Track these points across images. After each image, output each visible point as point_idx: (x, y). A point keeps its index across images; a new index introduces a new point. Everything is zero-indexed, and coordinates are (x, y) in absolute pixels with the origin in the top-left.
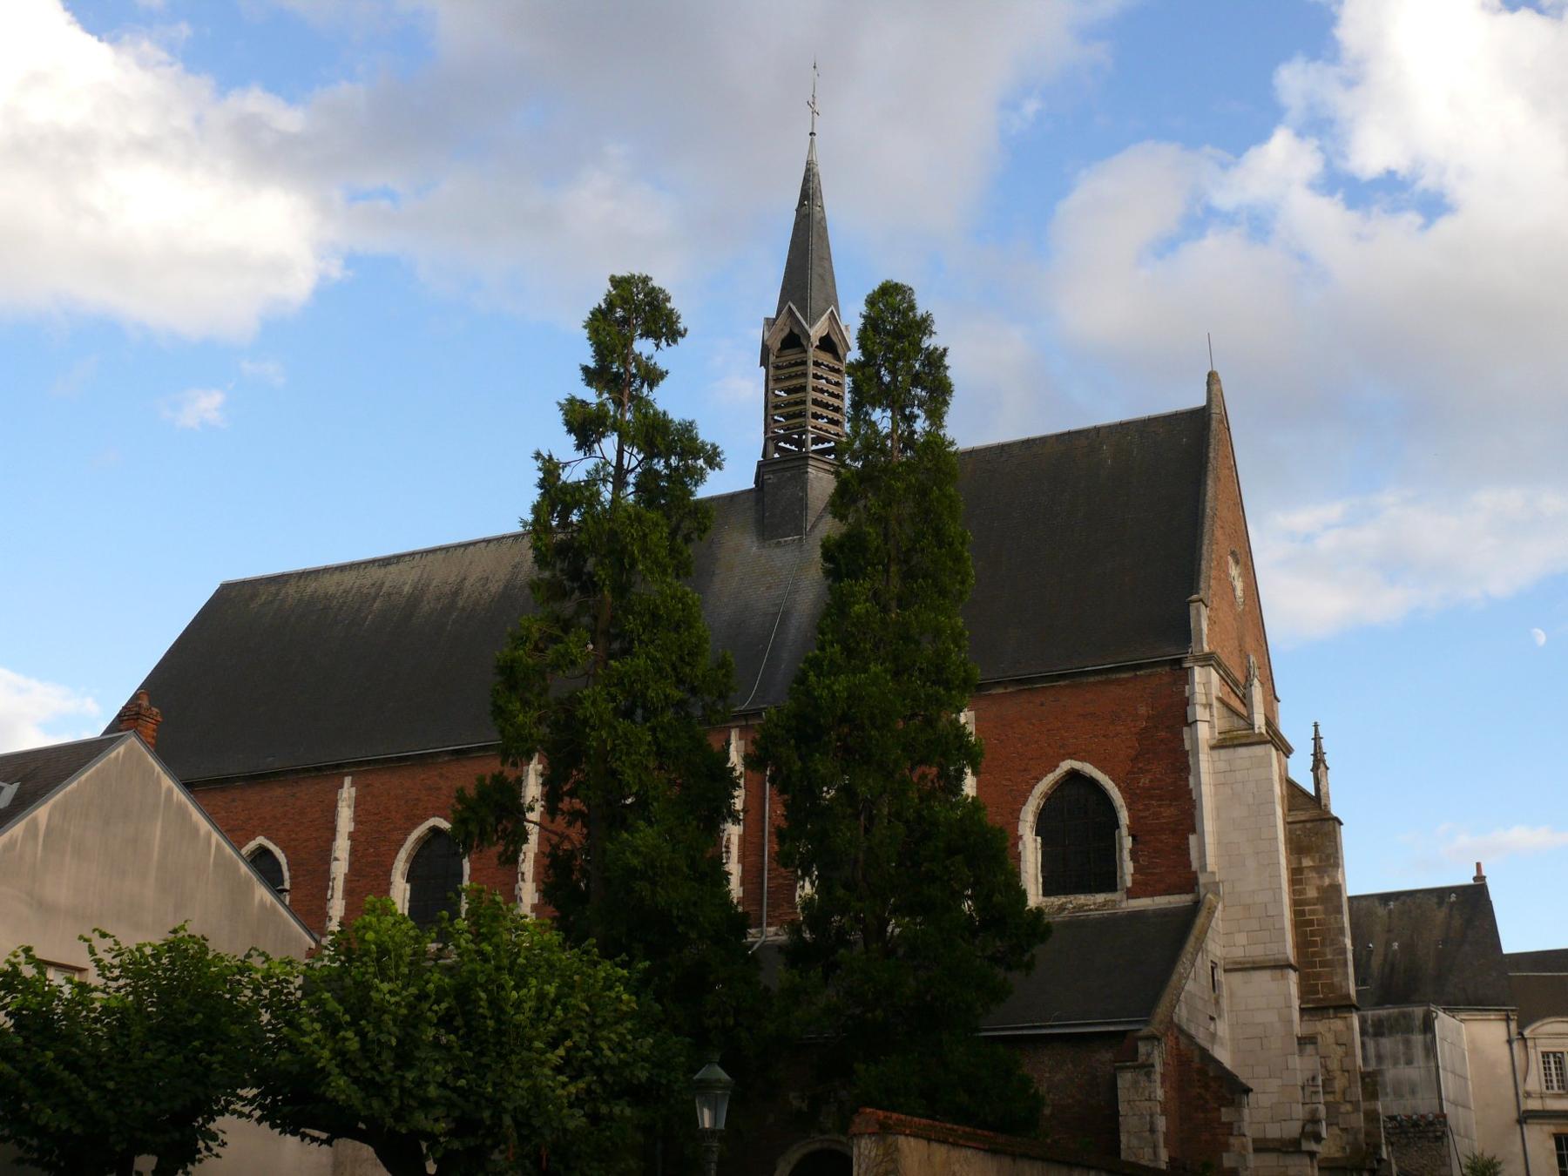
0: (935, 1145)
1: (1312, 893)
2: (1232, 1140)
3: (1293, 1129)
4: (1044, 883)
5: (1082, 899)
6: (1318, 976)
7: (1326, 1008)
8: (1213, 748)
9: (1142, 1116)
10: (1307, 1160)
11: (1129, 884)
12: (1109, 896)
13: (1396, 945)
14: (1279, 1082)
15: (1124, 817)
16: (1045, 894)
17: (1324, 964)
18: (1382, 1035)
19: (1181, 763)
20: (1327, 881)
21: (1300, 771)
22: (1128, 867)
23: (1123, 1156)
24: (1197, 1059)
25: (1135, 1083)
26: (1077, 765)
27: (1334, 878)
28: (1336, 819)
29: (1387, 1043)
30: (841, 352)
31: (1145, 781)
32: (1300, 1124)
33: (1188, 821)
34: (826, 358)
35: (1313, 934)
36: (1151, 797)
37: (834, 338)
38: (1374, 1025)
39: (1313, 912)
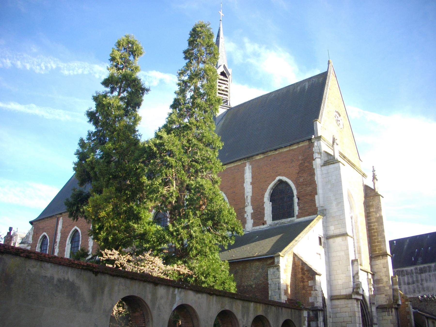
0: (258, 304)
2: (312, 292)
3: (349, 291)
5: (284, 220)
6: (376, 246)
7: (379, 256)
8: (322, 166)
9: (275, 284)
10: (355, 301)
15: (295, 193)
17: (378, 242)
18: (422, 273)
19: (312, 173)
20: (378, 215)
23: (269, 298)
29: (423, 275)
31: (301, 180)
33: (314, 192)
34: (222, 77)
36: (303, 185)
38: (420, 270)
39: (374, 226)
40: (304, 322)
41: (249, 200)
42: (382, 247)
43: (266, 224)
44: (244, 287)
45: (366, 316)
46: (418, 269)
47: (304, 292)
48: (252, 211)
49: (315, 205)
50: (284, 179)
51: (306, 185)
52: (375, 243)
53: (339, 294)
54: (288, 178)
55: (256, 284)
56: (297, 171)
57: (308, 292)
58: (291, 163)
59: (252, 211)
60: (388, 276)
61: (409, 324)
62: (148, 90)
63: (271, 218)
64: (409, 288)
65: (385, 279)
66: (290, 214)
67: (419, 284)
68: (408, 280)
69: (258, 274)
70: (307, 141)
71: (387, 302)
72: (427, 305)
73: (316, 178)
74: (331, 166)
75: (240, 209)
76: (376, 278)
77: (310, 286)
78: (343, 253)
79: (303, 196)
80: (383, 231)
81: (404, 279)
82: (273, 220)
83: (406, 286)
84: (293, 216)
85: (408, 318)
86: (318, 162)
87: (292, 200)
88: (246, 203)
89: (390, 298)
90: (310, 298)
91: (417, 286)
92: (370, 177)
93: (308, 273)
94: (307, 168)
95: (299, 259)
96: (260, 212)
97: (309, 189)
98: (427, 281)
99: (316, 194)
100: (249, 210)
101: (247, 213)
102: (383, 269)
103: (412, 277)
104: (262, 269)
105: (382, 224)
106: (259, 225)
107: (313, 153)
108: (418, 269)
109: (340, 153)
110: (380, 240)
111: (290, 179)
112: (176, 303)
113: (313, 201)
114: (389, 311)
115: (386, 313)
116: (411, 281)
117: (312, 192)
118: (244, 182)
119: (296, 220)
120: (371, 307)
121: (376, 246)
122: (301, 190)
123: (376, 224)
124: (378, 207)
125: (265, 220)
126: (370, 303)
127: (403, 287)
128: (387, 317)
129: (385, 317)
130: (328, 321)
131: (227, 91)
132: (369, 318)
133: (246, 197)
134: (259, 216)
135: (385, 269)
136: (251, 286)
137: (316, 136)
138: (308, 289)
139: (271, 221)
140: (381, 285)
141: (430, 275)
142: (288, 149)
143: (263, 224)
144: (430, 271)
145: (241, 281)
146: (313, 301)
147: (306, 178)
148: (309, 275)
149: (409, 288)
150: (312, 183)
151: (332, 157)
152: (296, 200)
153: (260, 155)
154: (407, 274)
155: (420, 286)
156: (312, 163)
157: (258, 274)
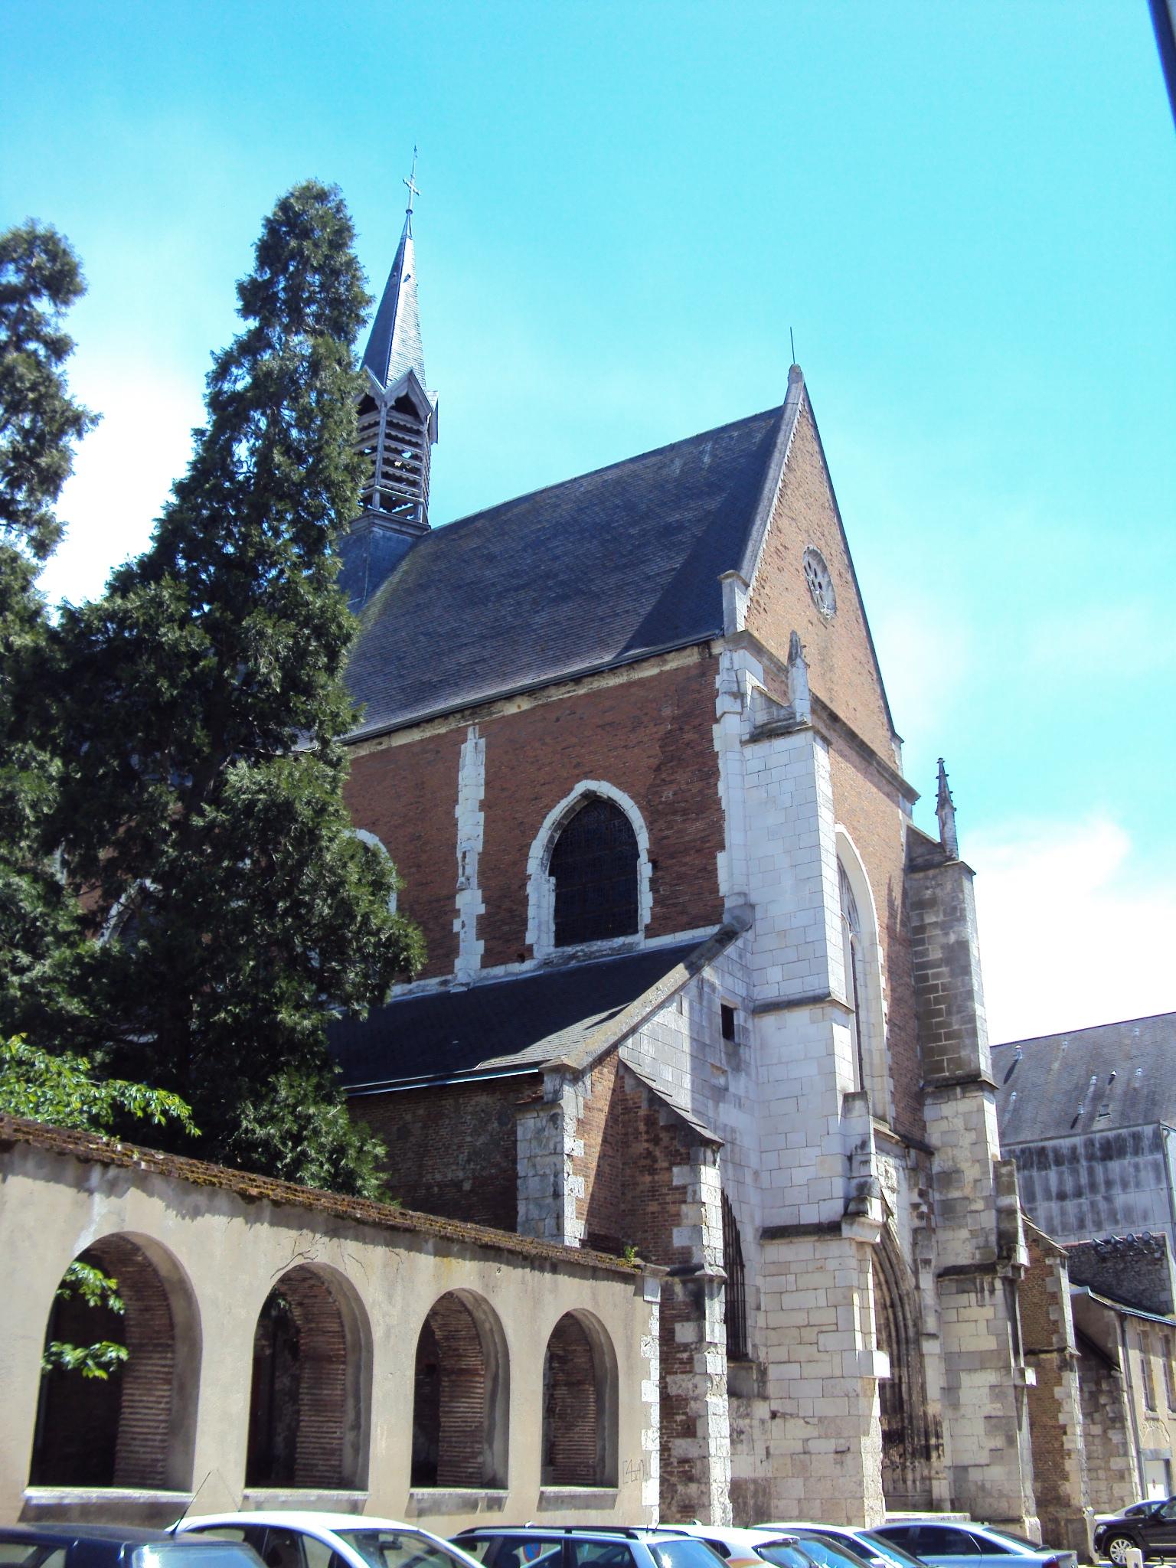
3: (833, 1209)
5: (598, 945)
8: (743, 743)
12: (629, 939)
13: (1139, 1072)
15: (643, 841)
16: (560, 941)
18: (1111, 1158)
19: (708, 769)
20: (952, 938)
21: (925, 820)
24: (644, 1105)
27: (959, 934)
29: (1115, 1166)
30: (422, 414)
31: (668, 794)
33: (713, 841)
35: (937, 1001)
36: (675, 813)
37: (414, 399)
38: (1102, 1148)
39: (937, 976)
40: (646, 1322)
41: (470, 869)
42: (963, 1053)
43: (532, 957)
44: (429, 1187)
45: (899, 1309)
46: (1097, 1145)
47: (653, 1207)
48: (482, 909)
49: (715, 889)
50: (605, 789)
51: (685, 812)
53: (795, 1222)
55: (475, 1178)
56: (655, 762)
57: (672, 1209)
58: (633, 730)
59: (482, 909)
60: (983, 1161)
61: (1054, 1339)
63: (552, 935)
64: (1063, 1213)
65: (971, 1172)
66: (627, 923)
67: (1099, 1198)
68: (1061, 1182)
69: (482, 1140)
70: (696, 649)
71: (978, 1256)
72: (1124, 1269)
73: (721, 786)
74: (780, 744)
75: (438, 900)
77: (677, 1188)
79: (672, 856)
80: (969, 995)
81: (1047, 1179)
83: (1054, 1206)
84: (636, 932)
85: (1052, 1317)
86: (728, 731)
88: (462, 879)
89: (987, 1241)
90: (675, 1231)
91: (1093, 1204)
93: (672, 1139)
94: (690, 752)
95: (640, 1083)
96: (511, 911)
97: (696, 827)
98: (1125, 1185)
99: (722, 847)
100: (470, 903)
101: (463, 917)
102: (967, 1134)
103: (1075, 1172)
104: (499, 1119)
105: (965, 970)
107: (715, 694)
108: (1097, 1145)
110: (956, 1027)
111: (624, 790)
112: (93, 1228)
113: (711, 872)
114: (982, 1290)
115: (973, 1295)
116: (1069, 1186)
117: (703, 840)
118: (456, 801)
119: (641, 942)
120: (916, 1273)
121: (943, 1051)
122: (669, 833)
124: (954, 908)
125: (528, 941)
127: (1043, 1207)
128: (975, 1312)
130: (749, 1322)
132: (908, 1316)
133: (459, 856)
134: (506, 928)
135: (971, 1136)
136: (457, 1184)
138: (669, 1199)
139: (552, 949)
140: (955, 1194)
141: (1137, 1167)
143: (522, 958)
144: (1137, 1151)
146: (686, 1243)
147: (684, 787)
148: (675, 1142)
149: (1063, 1213)
151: (783, 712)
152: (645, 869)
153: (519, 700)
154: (1058, 1162)
155: (1103, 1205)
156: (710, 732)
157: (482, 1140)
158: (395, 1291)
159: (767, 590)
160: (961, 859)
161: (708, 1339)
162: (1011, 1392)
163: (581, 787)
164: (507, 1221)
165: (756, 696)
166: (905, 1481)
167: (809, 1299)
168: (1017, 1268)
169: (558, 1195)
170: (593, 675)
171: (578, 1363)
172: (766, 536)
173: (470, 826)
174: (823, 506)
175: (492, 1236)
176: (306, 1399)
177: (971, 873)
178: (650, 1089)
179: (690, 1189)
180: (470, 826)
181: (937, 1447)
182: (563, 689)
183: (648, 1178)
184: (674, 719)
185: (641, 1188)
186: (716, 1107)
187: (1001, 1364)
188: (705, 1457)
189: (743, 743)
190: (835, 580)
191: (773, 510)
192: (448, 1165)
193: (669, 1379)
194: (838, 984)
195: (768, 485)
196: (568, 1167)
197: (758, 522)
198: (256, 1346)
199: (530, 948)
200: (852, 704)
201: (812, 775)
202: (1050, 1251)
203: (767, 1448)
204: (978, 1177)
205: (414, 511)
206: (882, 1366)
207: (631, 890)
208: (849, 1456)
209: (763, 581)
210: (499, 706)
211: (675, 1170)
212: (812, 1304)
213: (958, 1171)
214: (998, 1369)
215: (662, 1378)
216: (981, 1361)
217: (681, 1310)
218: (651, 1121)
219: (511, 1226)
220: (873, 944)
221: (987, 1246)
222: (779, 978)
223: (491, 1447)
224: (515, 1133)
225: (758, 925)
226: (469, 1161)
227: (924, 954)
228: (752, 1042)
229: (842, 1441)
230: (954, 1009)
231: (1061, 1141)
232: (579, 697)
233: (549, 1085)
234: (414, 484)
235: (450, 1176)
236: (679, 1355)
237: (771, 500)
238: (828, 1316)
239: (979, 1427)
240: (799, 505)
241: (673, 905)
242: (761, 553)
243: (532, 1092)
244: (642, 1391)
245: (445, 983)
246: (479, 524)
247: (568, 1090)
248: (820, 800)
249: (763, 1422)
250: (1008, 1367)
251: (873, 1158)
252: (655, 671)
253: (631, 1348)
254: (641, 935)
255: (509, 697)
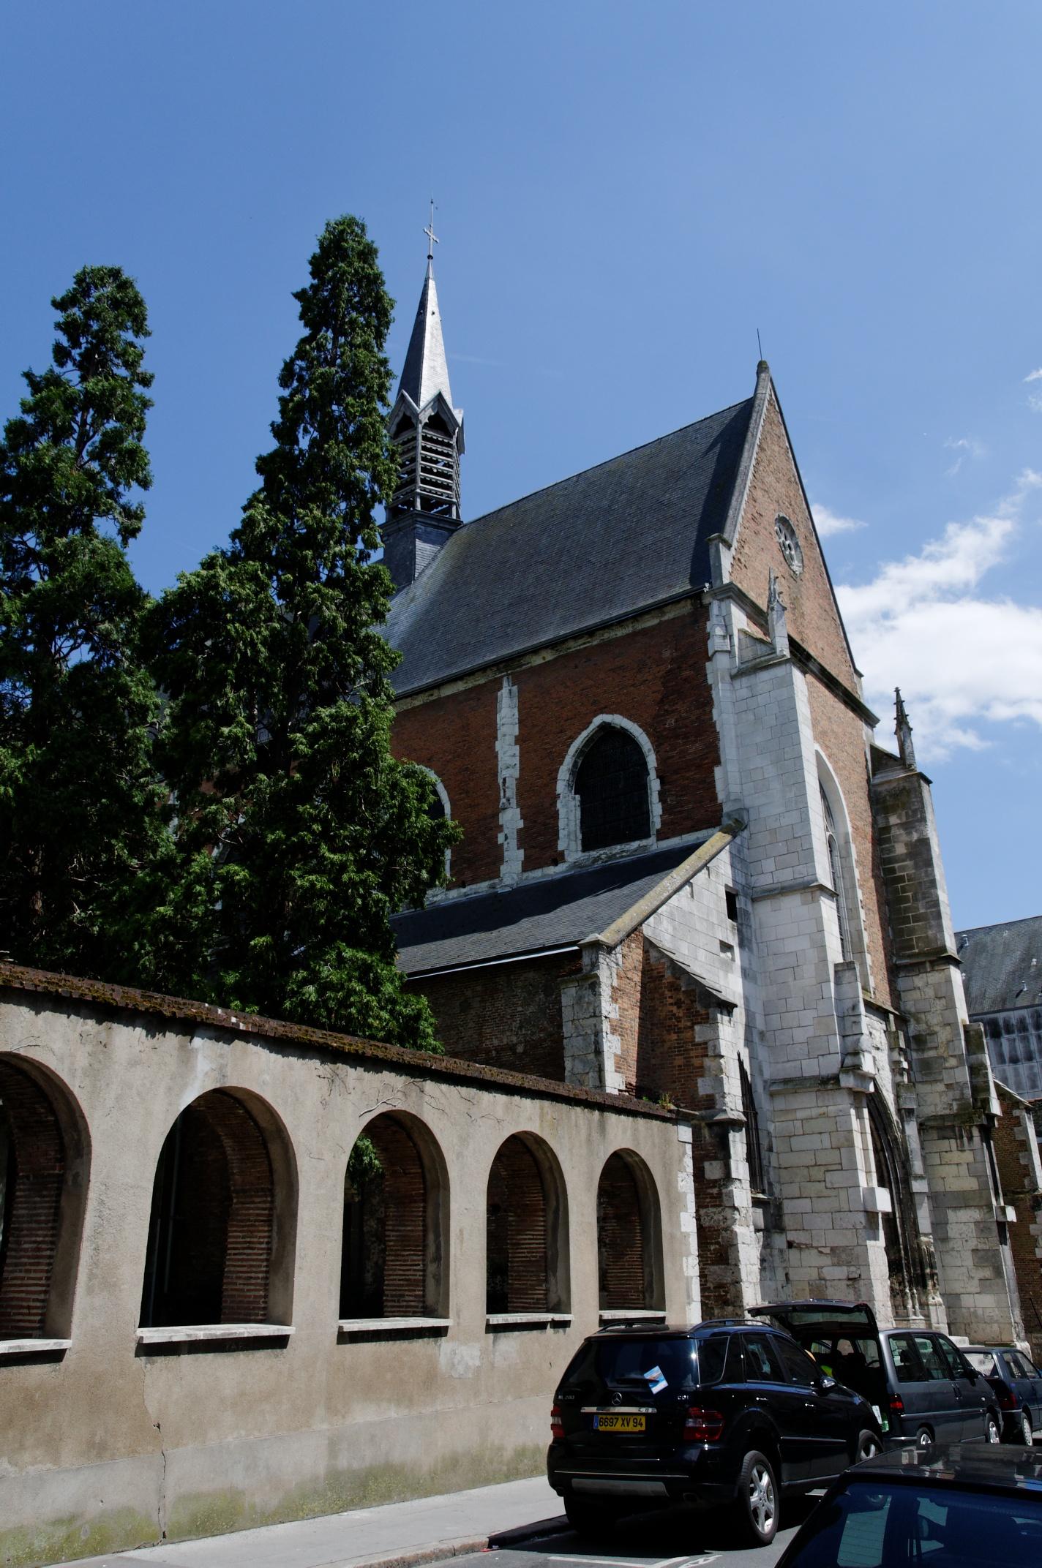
1: (900, 849)
2: (707, 1062)
4: (583, 840)
5: (617, 849)
11: (658, 826)
12: (644, 842)
14: (812, 1014)
15: (652, 761)
16: (586, 847)
17: (916, 919)
19: (705, 701)
20: (915, 836)
22: (656, 809)
24: (668, 974)
25: (579, 999)
26: (607, 718)
28: (922, 776)
30: (450, 429)
31: (671, 722)
32: (839, 1057)
33: (712, 757)
39: (903, 868)
40: (681, 1160)
41: (511, 791)
48: (521, 824)
50: (619, 720)
52: (906, 920)
53: (799, 1075)
54: (630, 718)
57: (696, 1062)
59: (521, 824)
60: (952, 1024)
61: (1026, 1181)
62: (152, 377)
68: (1013, 1049)
69: (531, 1009)
71: (955, 1107)
73: (715, 712)
74: (765, 675)
76: (913, 1029)
77: (699, 1044)
78: (804, 944)
82: (584, 851)
84: (647, 836)
85: (1023, 1162)
86: (718, 669)
87: (644, 788)
88: (503, 800)
90: (700, 1081)
92: (887, 722)
97: (694, 748)
99: (717, 762)
100: (511, 819)
101: (506, 831)
103: (1025, 1039)
106: (540, 866)
107: (707, 637)
109: (792, 642)
114: (961, 1137)
115: (953, 1141)
118: (496, 738)
119: (654, 845)
121: (912, 931)
123: (908, 863)
125: (560, 848)
126: (899, 1110)
128: (956, 1156)
129: (947, 1157)
131: (449, 477)
133: (500, 781)
134: (541, 839)
135: (940, 1004)
136: (512, 1048)
137: (717, 585)
138: (692, 1054)
142: (628, 630)
143: (555, 863)
145: (480, 1034)
146: (710, 1091)
150: (705, 734)
152: (655, 785)
154: (1009, 1031)
156: (704, 668)
157: (531, 1009)
158: (470, 1129)
159: (746, 550)
160: (918, 771)
161: (734, 1175)
162: (995, 1227)
163: (598, 720)
164: (557, 1073)
165: (742, 636)
166: (905, 1307)
167: (815, 1142)
168: (991, 1117)
169: (599, 1052)
170: (603, 628)
171: (626, 1187)
172: (744, 505)
173: (508, 755)
174: (789, 481)
175: (543, 1084)
176: (392, 1235)
177: (928, 782)
178: (672, 960)
179: (710, 1044)
180: (508, 755)
181: (932, 1275)
182: (580, 642)
183: (674, 1037)
184: (673, 660)
185: (667, 1045)
186: (726, 976)
187: (983, 1203)
188: (737, 1282)
189: (733, 677)
190: (801, 542)
191: (748, 483)
192: (503, 1032)
193: (702, 1212)
194: (824, 875)
195: (743, 464)
196: (606, 1026)
197: (736, 493)
198: (346, 1194)
199: (562, 853)
200: (820, 645)
201: (792, 699)
202: (1017, 1104)
203: (787, 1275)
204: (949, 1037)
205: (449, 511)
206: (883, 1201)
207: (650, 779)
208: (861, 1282)
209: (742, 542)
210: (527, 659)
211: (697, 1028)
212: (818, 1146)
213: (934, 1033)
214: (979, 1207)
215: (697, 1212)
216: (962, 1200)
217: (711, 1147)
218: (674, 987)
219: (561, 1078)
220: (847, 842)
221: (962, 1098)
222: (773, 869)
223: (555, 1275)
224: (560, 1002)
225: (752, 828)
226: (520, 1028)
227: (890, 850)
228: (752, 923)
229: (853, 1269)
230: (920, 896)
231: (1011, 1013)
232: (592, 647)
233: (586, 960)
234: (448, 487)
235: (505, 1041)
236: (710, 1191)
237: (747, 475)
238: (832, 1157)
239: (968, 1260)
240: (770, 479)
241: (680, 812)
242: (740, 520)
243: (572, 966)
244: (681, 1223)
245: (493, 887)
246: (508, 512)
247: (602, 959)
248: (800, 718)
249: (781, 1251)
250: (990, 1206)
251: (863, 1018)
252: (656, 621)
253: (671, 1184)
254: (653, 839)
255: (535, 650)
